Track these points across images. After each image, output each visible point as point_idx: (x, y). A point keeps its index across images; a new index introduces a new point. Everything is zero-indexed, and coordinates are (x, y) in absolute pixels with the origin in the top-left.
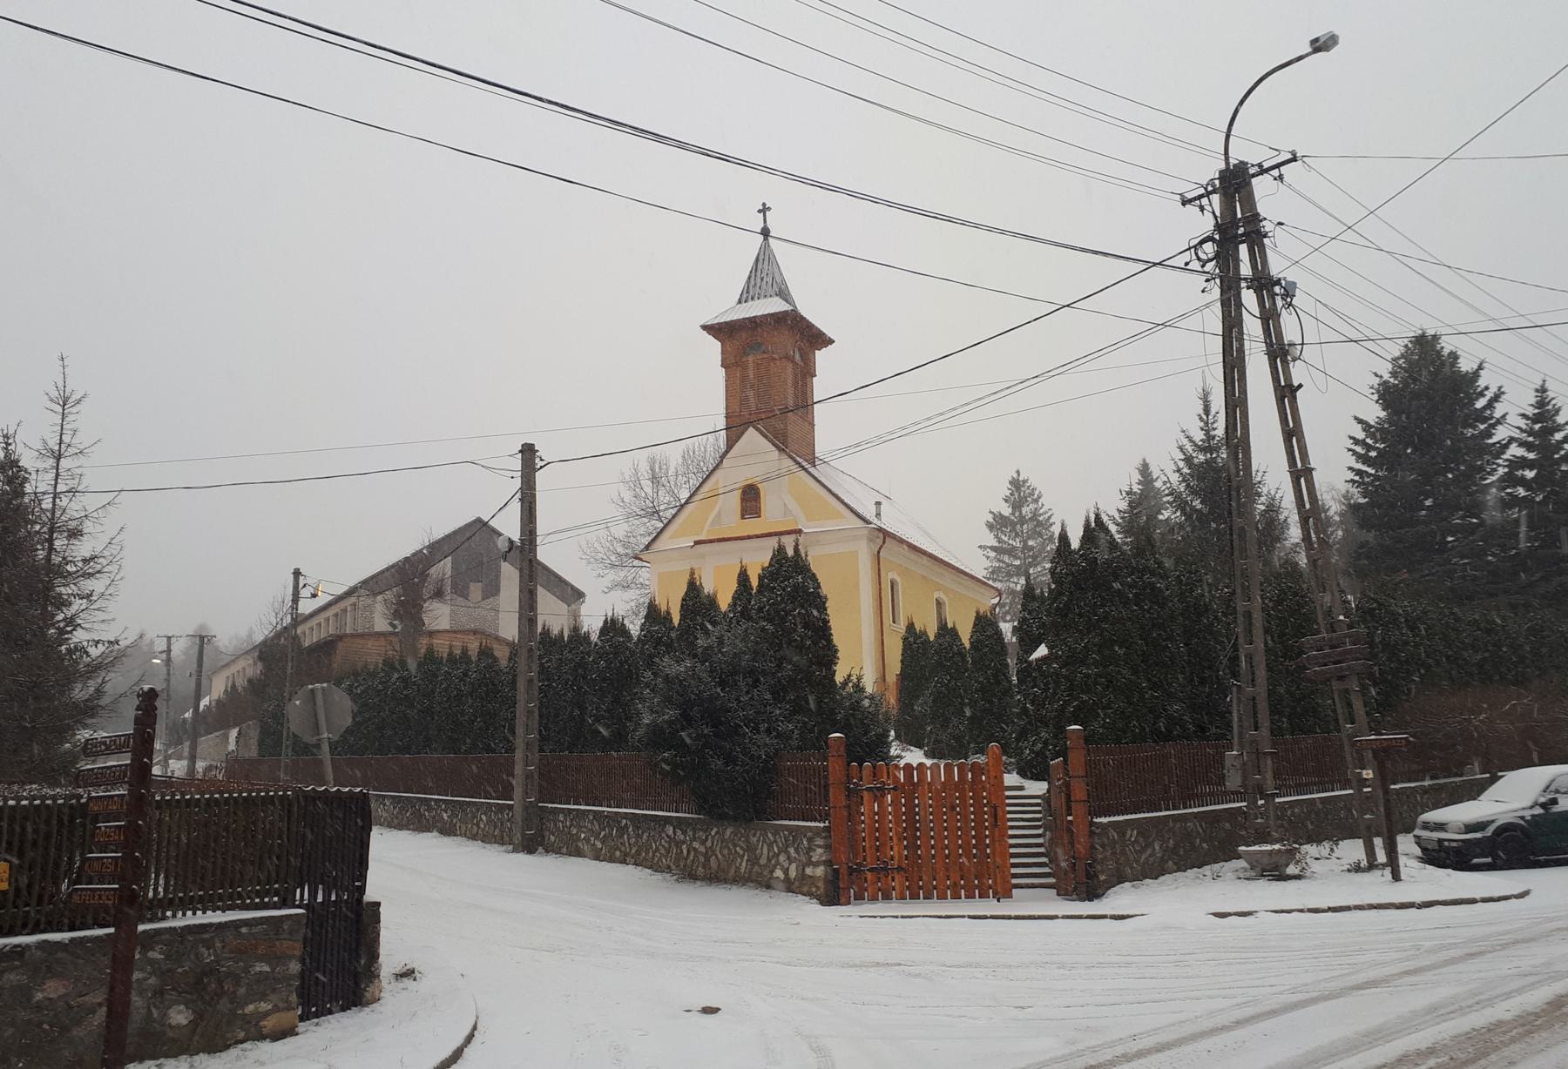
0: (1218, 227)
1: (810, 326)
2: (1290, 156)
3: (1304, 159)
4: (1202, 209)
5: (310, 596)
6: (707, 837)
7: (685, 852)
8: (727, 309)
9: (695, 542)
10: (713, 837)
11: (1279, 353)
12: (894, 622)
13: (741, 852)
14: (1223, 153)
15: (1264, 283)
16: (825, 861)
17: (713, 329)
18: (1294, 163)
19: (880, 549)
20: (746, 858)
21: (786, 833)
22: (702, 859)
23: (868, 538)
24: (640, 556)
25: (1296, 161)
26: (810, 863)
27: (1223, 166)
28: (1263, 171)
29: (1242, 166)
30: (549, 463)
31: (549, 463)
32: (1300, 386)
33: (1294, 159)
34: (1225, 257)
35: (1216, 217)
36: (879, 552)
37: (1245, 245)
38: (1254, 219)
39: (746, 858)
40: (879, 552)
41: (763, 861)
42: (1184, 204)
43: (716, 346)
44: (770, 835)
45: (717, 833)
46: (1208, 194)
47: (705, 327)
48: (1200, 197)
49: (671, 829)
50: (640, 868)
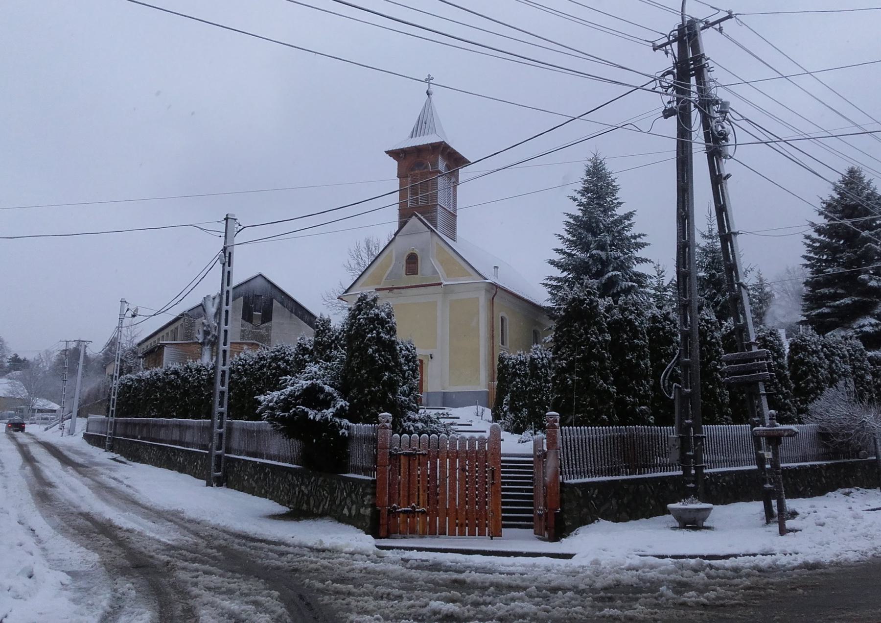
0: (676, 65)
1: (455, 153)
2: (727, 14)
3: (737, 16)
4: (667, 53)
5: (131, 316)
6: (309, 483)
7: (297, 493)
8: (404, 141)
9: (376, 289)
10: (312, 483)
11: (715, 153)
12: (503, 344)
13: (327, 495)
14: (681, 11)
15: (706, 103)
16: (371, 505)
17: (391, 153)
18: (729, 20)
19: (494, 296)
20: (329, 499)
21: (351, 483)
22: (306, 498)
23: (486, 290)
24: (342, 297)
25: (731, 18)
26: (363, 505)
27: (680, 22)
28: (708, 25)
29: (692, 23)
30: (244, 227)
31: (244, 227)
32: (728, 176)
33: (730, 17)
34: (681, 90)
35: (675, 58)
36: (493, 299)
37: (694, 77)
38: (699, 58)
39: (329, 499)
40: (493, 299)
41: (337, 502)
42: (655, 50)
43: (394, 164)
44: (342, 484)
45: (314, 480)
46: (669, 43)
47: (387, 152)
48: (665, 45)
49: (291, 476)
50: (272, 501)
